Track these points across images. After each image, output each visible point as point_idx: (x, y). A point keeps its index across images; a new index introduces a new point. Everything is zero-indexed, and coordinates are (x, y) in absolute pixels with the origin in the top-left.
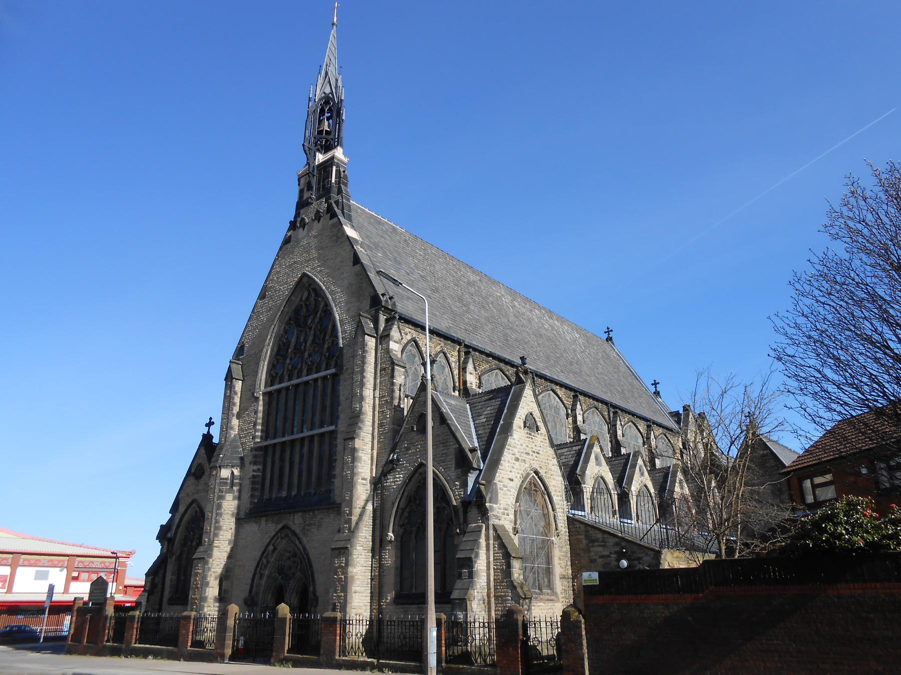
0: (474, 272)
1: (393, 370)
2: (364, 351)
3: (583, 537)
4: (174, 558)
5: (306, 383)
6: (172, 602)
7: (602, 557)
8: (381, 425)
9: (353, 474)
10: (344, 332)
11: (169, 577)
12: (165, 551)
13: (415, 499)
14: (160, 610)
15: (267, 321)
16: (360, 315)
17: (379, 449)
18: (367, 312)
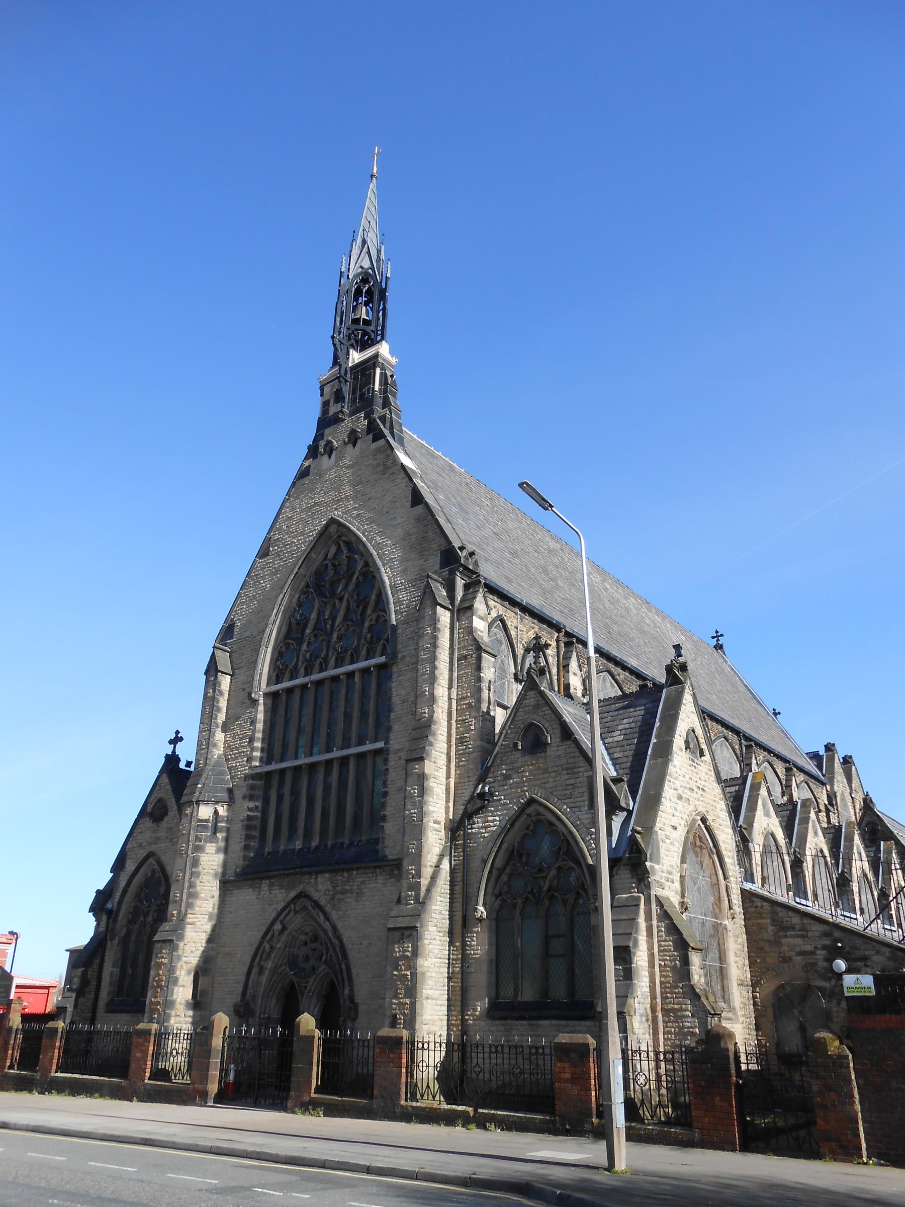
0: (552, 537)
1: (479, 659)
2: (435, 629)
3: (768, 921)
4: (116, 941)
5: (335, 679)
6: (113, 1008)
7: (802, 953)
8: (461, 741)
9: (421, 814)
10: (398, 602)
11: (109, 970)
12: (102, 929)
13: (520, 856)
14: (92, 1021)
15: (272, 588)
16: (428, 576)
17: (459, 777)
18: (435, 573)
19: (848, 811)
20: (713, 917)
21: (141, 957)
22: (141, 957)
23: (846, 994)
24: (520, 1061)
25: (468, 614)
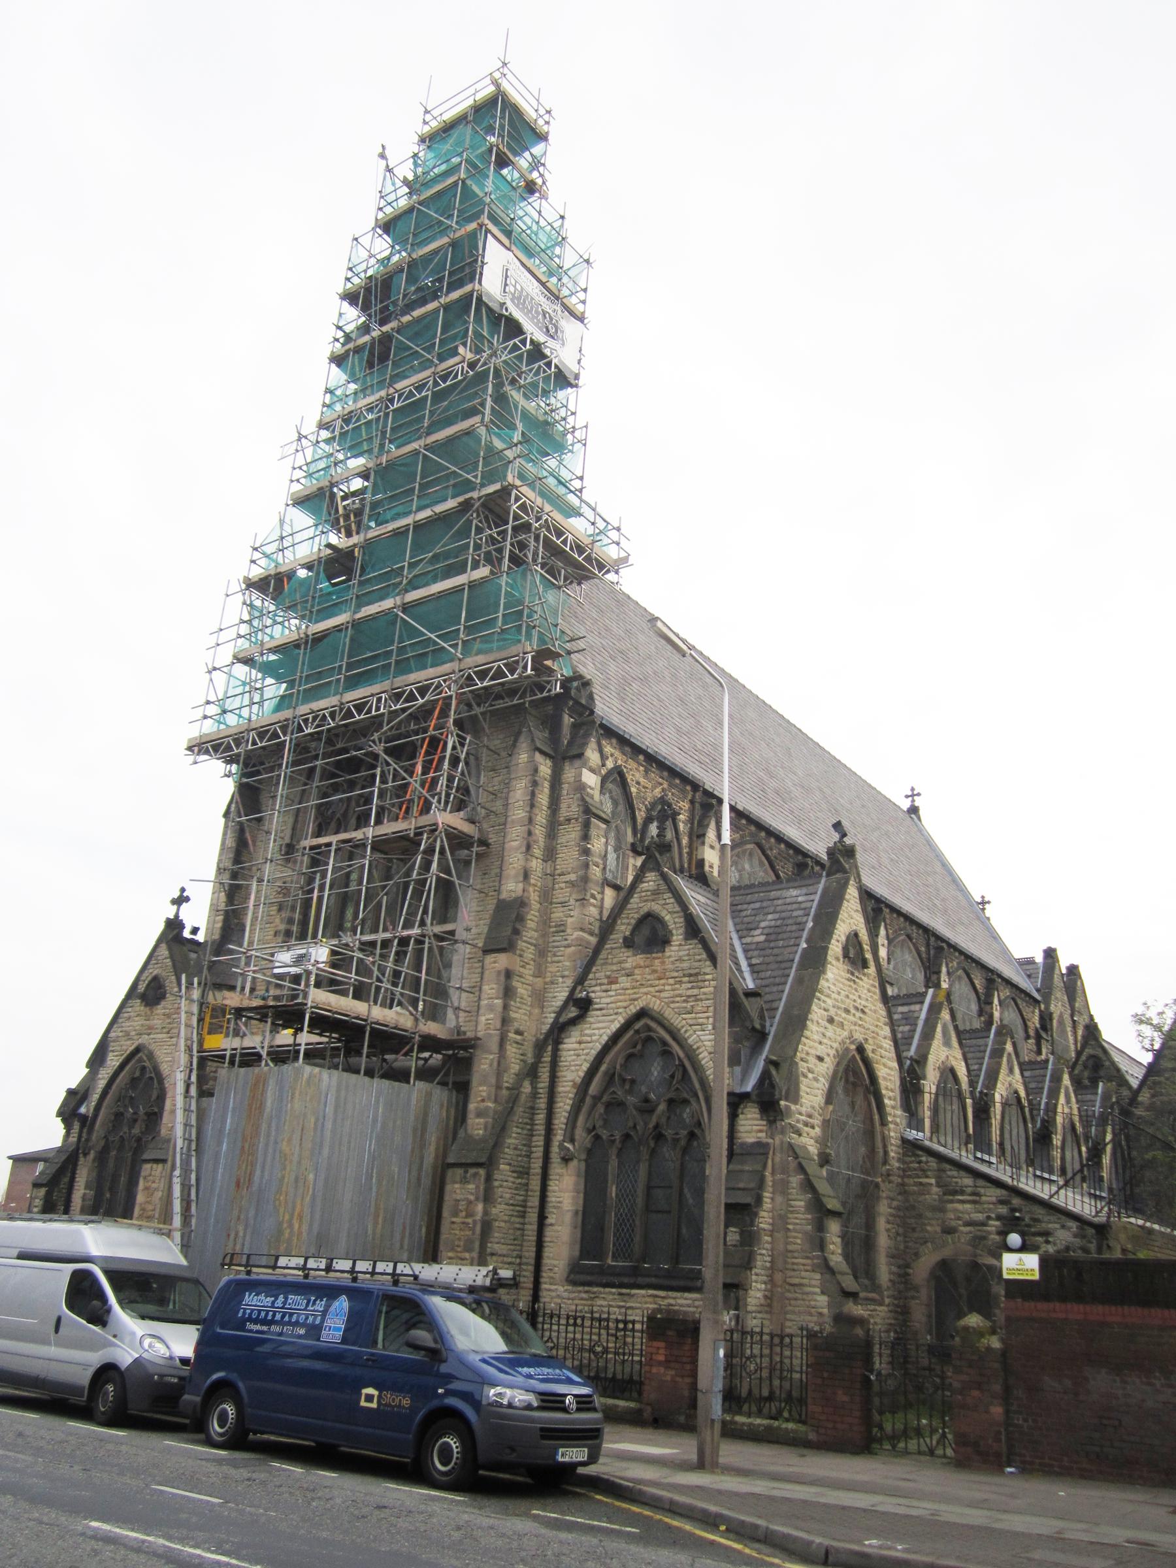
3: (933, 1181)
12: (73, 1139)
19: (1067, 1039)
20: (862, 1173)
23: (1005, 1276)
24: (604, 1336)
25: (577, 763)
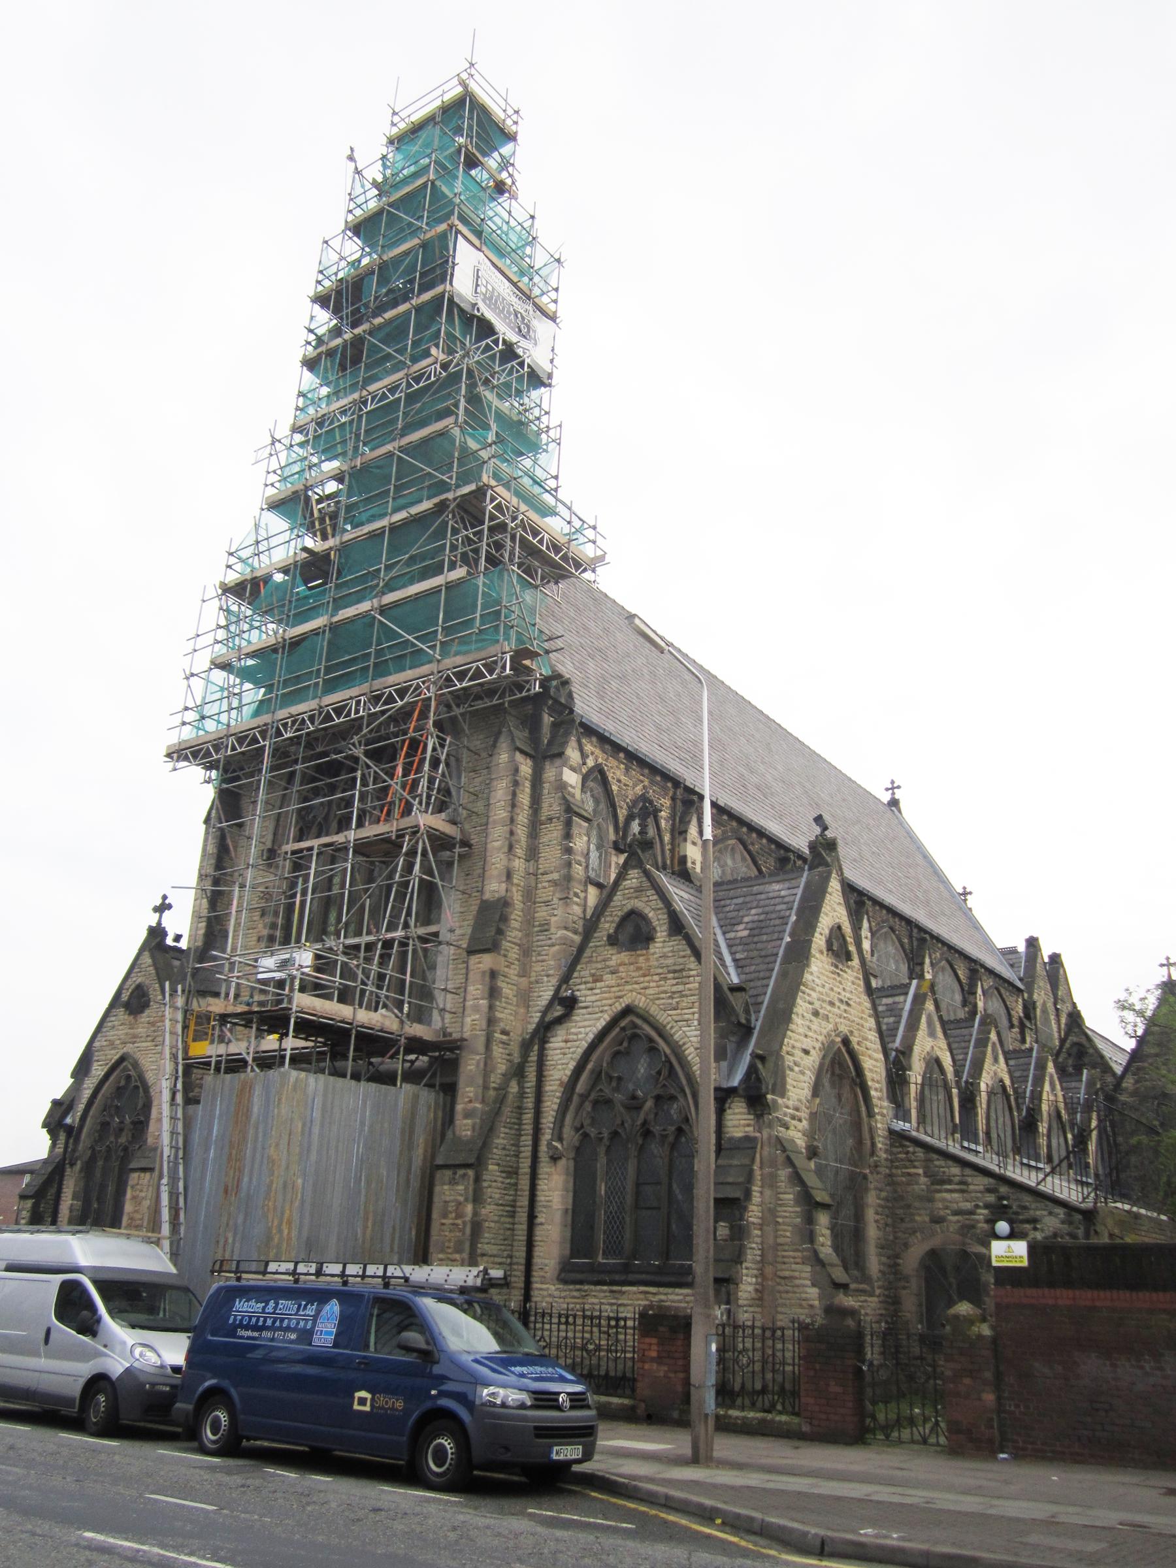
1: (568, 824)
3: (921, 1171)
12: (59, 1150)
20: (850, 1164)
21: (111, 1189)
22: (111, 1189)
24: (596, 1334)
25: (558, 762)
